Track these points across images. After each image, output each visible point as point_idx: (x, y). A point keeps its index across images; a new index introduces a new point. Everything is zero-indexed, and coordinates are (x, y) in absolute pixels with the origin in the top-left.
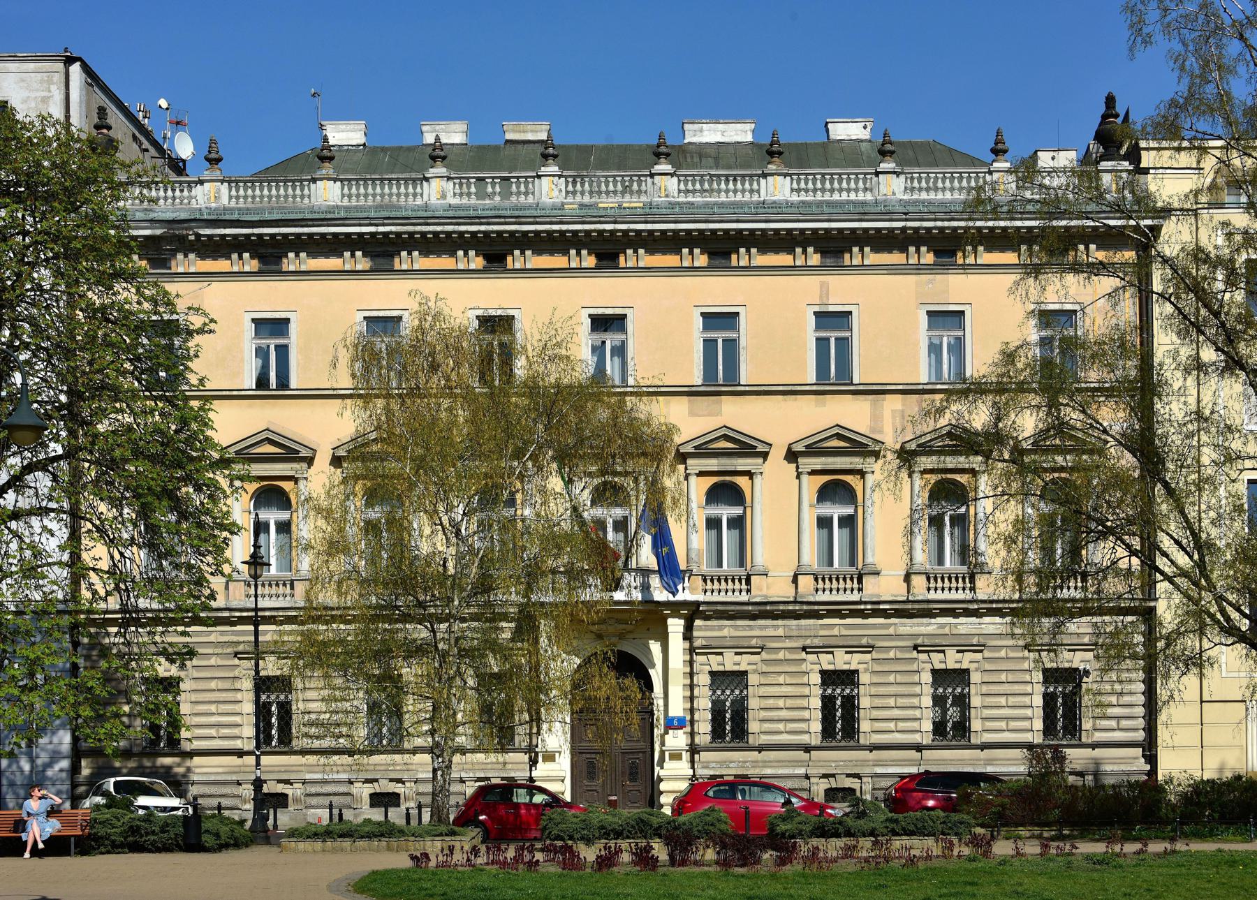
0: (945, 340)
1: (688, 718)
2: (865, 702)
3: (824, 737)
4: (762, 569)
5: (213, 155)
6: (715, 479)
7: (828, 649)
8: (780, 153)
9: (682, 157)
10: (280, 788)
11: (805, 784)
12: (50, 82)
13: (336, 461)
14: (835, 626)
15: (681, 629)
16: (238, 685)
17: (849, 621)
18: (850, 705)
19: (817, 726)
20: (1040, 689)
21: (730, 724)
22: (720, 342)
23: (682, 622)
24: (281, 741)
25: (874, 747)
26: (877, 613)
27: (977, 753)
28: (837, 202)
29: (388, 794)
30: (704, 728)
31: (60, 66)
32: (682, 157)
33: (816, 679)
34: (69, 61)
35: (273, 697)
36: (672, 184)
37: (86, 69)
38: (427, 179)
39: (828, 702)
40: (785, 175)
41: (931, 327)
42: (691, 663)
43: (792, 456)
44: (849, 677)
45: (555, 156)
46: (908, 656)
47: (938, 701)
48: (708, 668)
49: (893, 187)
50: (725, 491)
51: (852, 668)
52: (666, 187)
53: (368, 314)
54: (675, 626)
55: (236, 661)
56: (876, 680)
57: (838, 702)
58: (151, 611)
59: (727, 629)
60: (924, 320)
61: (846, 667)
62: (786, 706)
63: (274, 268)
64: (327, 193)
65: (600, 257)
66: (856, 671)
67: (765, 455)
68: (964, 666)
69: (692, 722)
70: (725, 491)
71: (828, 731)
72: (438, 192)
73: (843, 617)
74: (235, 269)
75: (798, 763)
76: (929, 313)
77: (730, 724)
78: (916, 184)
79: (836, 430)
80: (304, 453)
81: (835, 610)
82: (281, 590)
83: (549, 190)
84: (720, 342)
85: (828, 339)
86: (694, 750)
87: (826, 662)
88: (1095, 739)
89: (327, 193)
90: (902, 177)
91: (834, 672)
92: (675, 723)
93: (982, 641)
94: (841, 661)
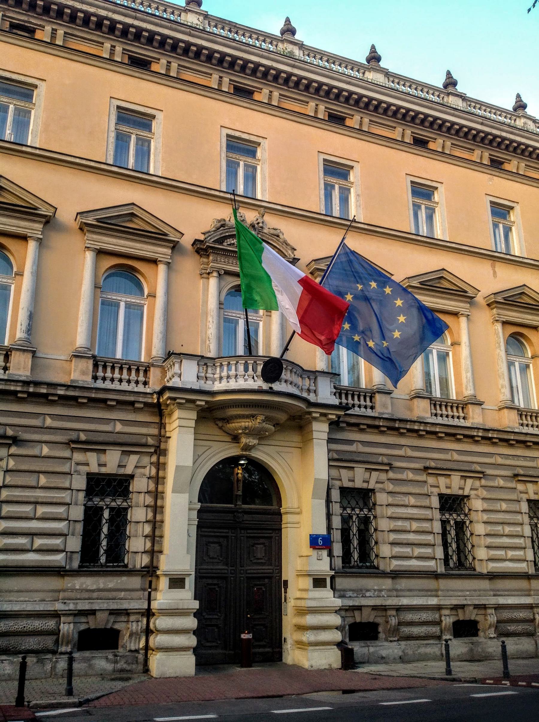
3: (83, 560)
7: (96, 445)
11: (51, 624)
29: (470, 621)
33: (80, 483)
39: (92, 516)
46: (510, 485)
51: (371, 486)
57: (106, 514)
76: (411, 181)
87: (93, 462)
92: (320, 542)
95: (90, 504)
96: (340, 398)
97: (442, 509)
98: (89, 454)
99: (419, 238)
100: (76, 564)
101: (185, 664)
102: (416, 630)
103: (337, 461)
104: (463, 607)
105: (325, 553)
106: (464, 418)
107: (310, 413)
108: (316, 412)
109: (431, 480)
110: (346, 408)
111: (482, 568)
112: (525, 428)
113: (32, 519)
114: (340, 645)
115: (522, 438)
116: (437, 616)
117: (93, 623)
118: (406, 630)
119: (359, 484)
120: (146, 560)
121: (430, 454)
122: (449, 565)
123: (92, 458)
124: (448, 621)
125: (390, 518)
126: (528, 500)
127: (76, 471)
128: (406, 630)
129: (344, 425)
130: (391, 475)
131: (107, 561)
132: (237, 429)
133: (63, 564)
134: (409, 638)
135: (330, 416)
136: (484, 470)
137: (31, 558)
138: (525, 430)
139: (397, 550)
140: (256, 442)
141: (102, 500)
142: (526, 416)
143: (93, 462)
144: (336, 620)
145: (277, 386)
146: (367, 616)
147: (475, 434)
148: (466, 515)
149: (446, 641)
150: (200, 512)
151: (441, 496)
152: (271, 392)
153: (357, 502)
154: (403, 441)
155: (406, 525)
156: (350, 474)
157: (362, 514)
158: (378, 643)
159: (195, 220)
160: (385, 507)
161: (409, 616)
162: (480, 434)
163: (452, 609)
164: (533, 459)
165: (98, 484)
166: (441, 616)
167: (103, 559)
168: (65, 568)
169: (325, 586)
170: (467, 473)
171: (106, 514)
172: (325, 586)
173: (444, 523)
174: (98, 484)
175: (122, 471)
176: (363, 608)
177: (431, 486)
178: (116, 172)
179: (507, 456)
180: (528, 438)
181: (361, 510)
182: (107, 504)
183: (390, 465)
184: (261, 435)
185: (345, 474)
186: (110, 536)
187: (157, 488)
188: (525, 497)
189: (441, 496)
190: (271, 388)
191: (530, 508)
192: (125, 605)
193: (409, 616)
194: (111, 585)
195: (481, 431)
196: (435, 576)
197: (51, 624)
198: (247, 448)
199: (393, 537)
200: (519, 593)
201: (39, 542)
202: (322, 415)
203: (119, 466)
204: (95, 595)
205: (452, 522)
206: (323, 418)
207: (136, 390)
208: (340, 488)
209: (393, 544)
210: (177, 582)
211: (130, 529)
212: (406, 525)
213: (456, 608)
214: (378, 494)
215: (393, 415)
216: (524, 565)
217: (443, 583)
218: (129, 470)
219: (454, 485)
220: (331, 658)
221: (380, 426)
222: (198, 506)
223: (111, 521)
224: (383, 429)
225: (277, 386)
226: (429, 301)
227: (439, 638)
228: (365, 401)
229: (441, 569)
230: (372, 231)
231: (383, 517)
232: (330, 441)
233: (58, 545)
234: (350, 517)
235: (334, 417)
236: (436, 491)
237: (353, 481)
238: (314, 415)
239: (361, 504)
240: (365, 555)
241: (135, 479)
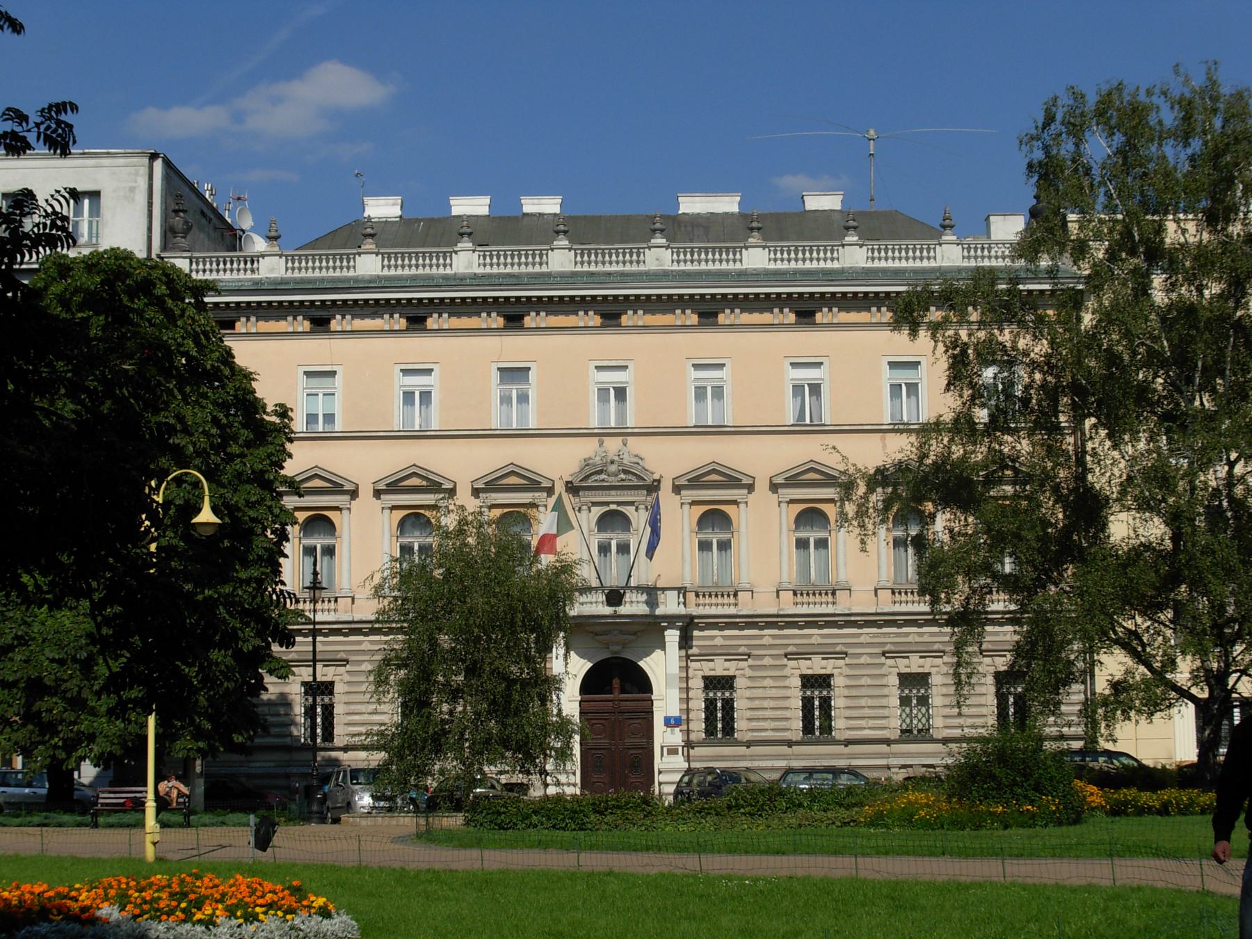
0: (514, 392)
1: (684, 717)
4: (748, 586)
5: (273, 234)
6: (606, 509)
7: (902, 653)
8: (951, 227)
9: (681, 230)
12: (137, 174)
13: (378, 494)
14: (815, 635)
15: (677, 639)
16: (786, 683)
17: (826, 631)
20: (896, 692)
21: (720, 719)
22: (709, 389)
23: (678, 633)
24: (325, 739)
26: (753, 625)
27: (742, 750)
28: (537, 274)
30: (698, 727)
31: (146, 160)
32: (681, 230)
34: (153, 157)
35: (817, 693)
36: (667, 255)
37: (168, 164)
38: (456, 252)
39: (807, 704)
40: (764, 247)
41: (502, 381)
42: (687, 667)
43: (677, 489)
44: (823, 681)
45: (855, 228)
46: (877, 661)
47: (905, 701)
48: (896, 670)
49: (756, 258)
50: (714, 518)
51: (828, 672)
52: (659, 257)
53: (404, 367)
54: (672, 636)
55: (785, 661)
58: (1010, 612)
59: (718, 638)
60: (495, 376)
61: (921, 670)
62: (768, 705)
63: (614, 322)
64: (368, 265)
65: (701, 315)
66: (929, 674)
69: (688, 720)
70: (714, 518)
71: (808, 728)
72: (465, 261)
73: (821, 627)
74: (679, 323)
76: (889, 363)
77: (720, 719)
78: (876, 254)
80: (745, 481)
81: (812, 622)
82: (824, 599)
83: (561, 259)
84: (709, 389)
85: (705, 388)
86: (689, 744)
87: (904, 666)
89: (368, 265)
90: (865, 248)
91: (812, 676)
92: (672, 722)
93: (844, 649)
94: (817, 666)
111: (937, 734)
119: (915, 669)
130: (847, 660)
138: (897, 608)
139: (754, 724)
165: (810, 681)
170: (828, 654)
174: (810, 681)
178: (800, 429)
189: (803, 677)
223: (821, 706)
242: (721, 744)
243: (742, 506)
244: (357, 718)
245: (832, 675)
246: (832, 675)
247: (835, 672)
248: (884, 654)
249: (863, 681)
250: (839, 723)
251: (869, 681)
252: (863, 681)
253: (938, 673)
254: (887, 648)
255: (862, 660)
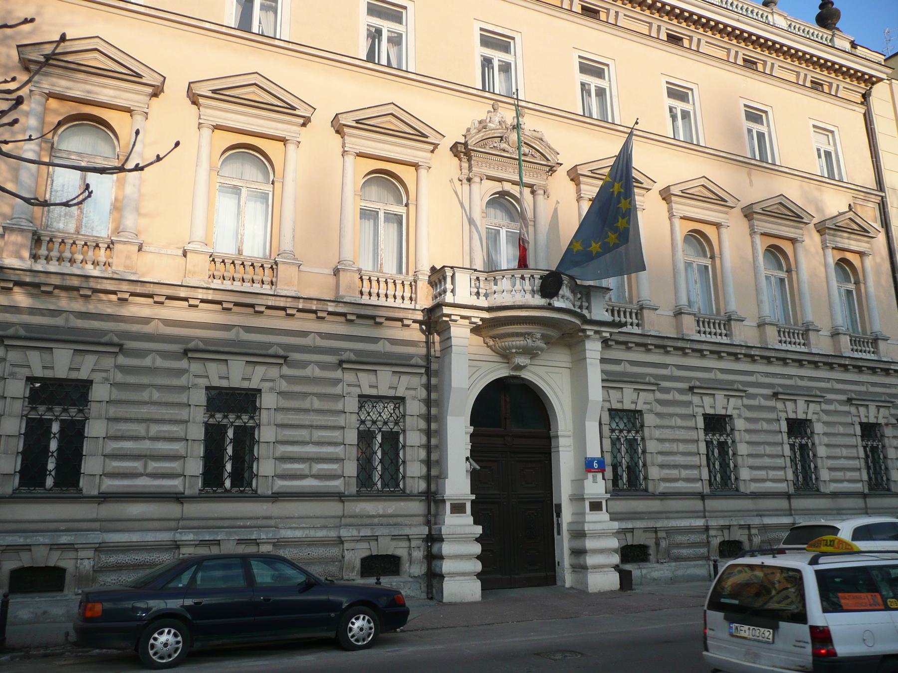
2: (266, 434)
3: (206, 484)
7: (708, 388)
10: (54, 559)
11: (334, 551)
18: (246, 439)
19: (195, 467)
20: (199, 415)
25: (277, 497)
27: (654, 505)
29: (47, 569)
33: (200, 397)
39: (214, 436)
48: (357, 391)
56: (283, 403)
57: (230, 433)
67: (306, 122)
68: (254, 385)
71: (212, 474)
75: (694, 514)
79: (391, 109)
88: (275, 489)
92: (596, 465)
95: (211, 421)
96: (613, 315)
97: (707, 430)
98: (360, 375)
99: (277, 42)
100: (354, 489)
101: (472, 590)
102: (684, 552)
103: (611, 380)
104: (729, 527)
105: (600, 476)
106: (638, 325)
107: (584, 331)
108: (590, 330)
109: (196, 367)
110: (621, 325)
112: (784, 345)
113: (144, 438)
114: (616, 567)
115: (782, 355)
116: (705, 536)
117: (26, 560)
118: (675, 551)
119: (628, 406)
120: (422, 486)
121: (253, 335)
122: (618, 486)
123: (34, 358)
124: (716, 542)
125: (658, 440)
126: (609, 410)
127: (10, 374)
128: (675, 551)
129: (613, 343)
130: (122, 360)
131: (232, 485)
132: (510, 348)
133: (181, 489)
134: (678, 559)
135: (604, 334)
136: (893, 400)
137: (309, 483)
139: (666, 472)
140: (527, 361)
141: (50, 410)
142: (798, 334)
143: (366, 383)
144: (614, 543)
145: (558, 303)
146: (639, 539)
147: (738, 351)
148: (809, 438)
149: (715, 561)
150: (472, 436)
151: (706, 416)
152: (550, 307)
153: (369, 413)
154: (668, 360)
155: (674, 447)
156: (371, 378)
157: (630, 436)
158: (648, 565)
159: (454, 118)
160: (104, 404)
161: (679, 539)
162: (743, 352)
163: (718, 529)
164: (890, 386)
166: (708, 537)
167: (228, 483)
168: (183, 493)
169: (601, 510)
171: (230, 433)
172: (601, 510)
173: (708, 444)
175: (74, 375)
176: (33, 548)
177: (349, 385)
179: (767, 375)
180: (704, 347)
181: (629, 431)
182: (232, 421)
183: (121, 346)
184: (531, 353)
185: (614, 395)
186: (235, 458)
187: (429, 412)
188: (203, 382)
189: (706, 416)
190: (550, 304)
191: (862, 431)
192: (407, 531)
193: (679, 539)
194: (390, 511)
195: (315, 302)
196: (340, 497)
197: (334, 551)
198: (519, 368)
199: (660, 459)
200: (691, 515)
201: (153, 466)
202: (596, 332)
203: (70, 369)
204: (376, 520)
205: (715, 443)
206: (597, 336)
207: (402, 306)
208: (609, 410)
209: (662, 466)
210: (458, 508)
211: (87, 447)
212: (674, 447)
213: (722, 528)
214: (645, 416)
215: (746, 342)
216: (784, 485)
217: (711, 504)
218: (83, 375)
219: (718, 404)
220: (612, 580)
221: (737, 354)
222: (471, 429)
223: (236, 441)
224: (650, 347)
225: (558, 303)
226: (845, 241)
227: (707, 558)
228: (631, 318)
229: (707, 490)
230: (425, 81)
231: (651, 439)
232: (603, 361)
233: (336, 470)
234: (618, 439)
235: (607, 335)
236: (700, 411)
237: (622, 402)
238: (588, 333)
239: (630, 426)
240: (726, 478)
241: (263, 395)
242: (227, 496)
243: (291, 147)
244: (129, 445)
245: (91, 382)
246: (259, 391)
247: (265, 386)
248: (691, 389)
249: (672, 422)
250: (265, 467)
251: (317, 404)
252: (672, 422)
253: (272, 389)
254: (345, 356)
255: (308, 372)
